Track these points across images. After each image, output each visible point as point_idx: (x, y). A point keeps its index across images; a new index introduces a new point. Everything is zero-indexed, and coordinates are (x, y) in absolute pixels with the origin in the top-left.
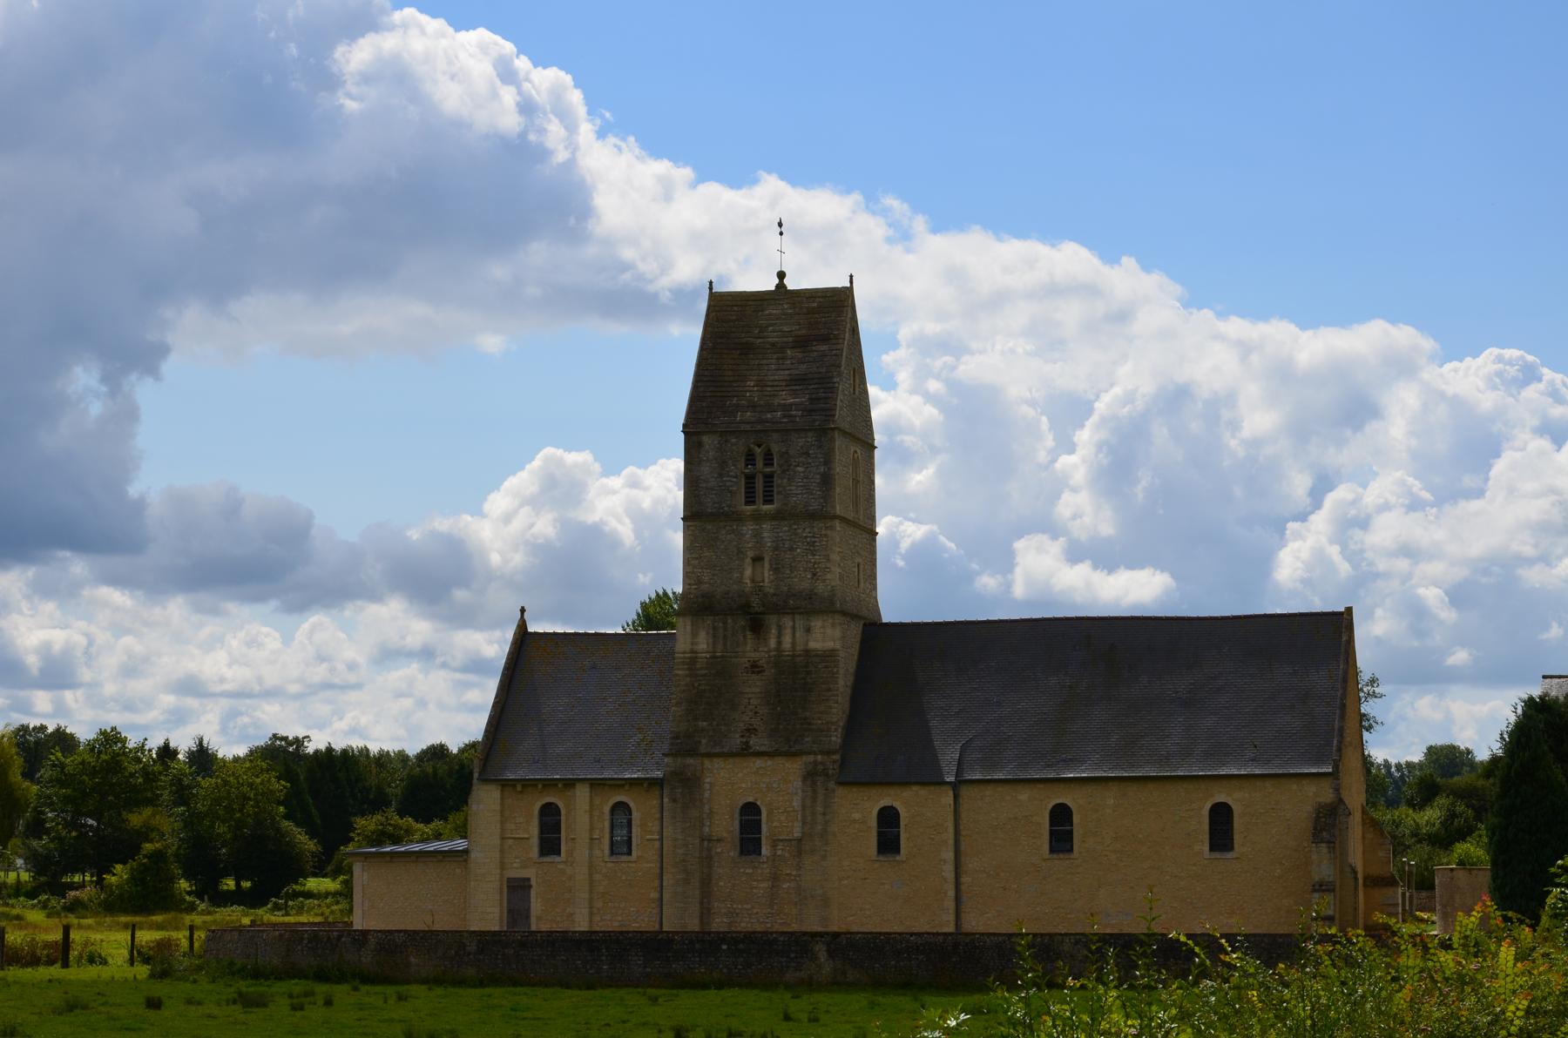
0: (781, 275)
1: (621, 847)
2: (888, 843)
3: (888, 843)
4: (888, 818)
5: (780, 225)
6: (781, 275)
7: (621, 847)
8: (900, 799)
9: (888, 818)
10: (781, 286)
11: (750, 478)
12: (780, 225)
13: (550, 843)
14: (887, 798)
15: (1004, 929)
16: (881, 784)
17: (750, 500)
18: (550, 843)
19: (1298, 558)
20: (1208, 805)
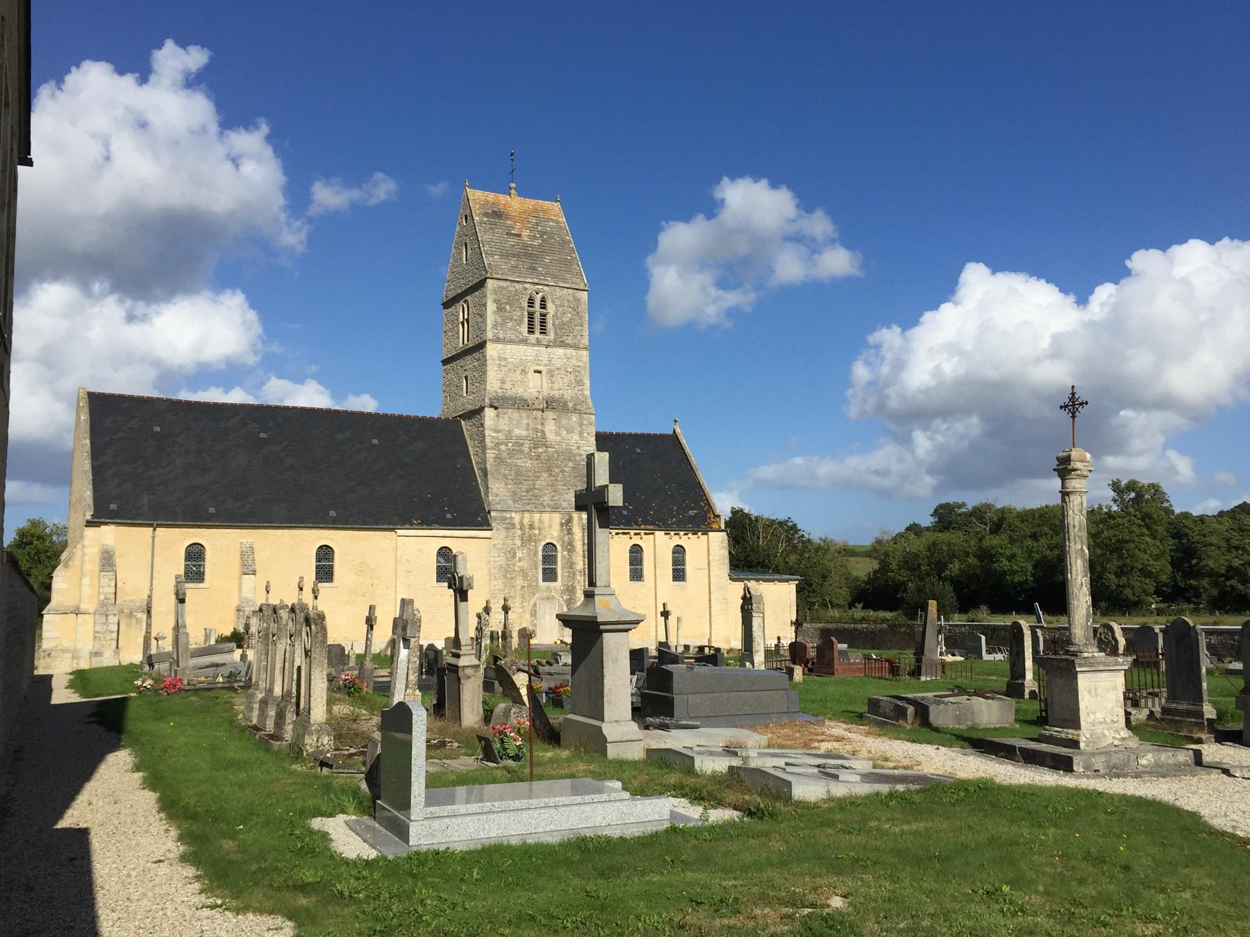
2: (325, 572)
3: (325, 572)
7: (637, 575)
8: (337, 539)
9: (325, 554)
11: (531, 316)
17: (531, 331)
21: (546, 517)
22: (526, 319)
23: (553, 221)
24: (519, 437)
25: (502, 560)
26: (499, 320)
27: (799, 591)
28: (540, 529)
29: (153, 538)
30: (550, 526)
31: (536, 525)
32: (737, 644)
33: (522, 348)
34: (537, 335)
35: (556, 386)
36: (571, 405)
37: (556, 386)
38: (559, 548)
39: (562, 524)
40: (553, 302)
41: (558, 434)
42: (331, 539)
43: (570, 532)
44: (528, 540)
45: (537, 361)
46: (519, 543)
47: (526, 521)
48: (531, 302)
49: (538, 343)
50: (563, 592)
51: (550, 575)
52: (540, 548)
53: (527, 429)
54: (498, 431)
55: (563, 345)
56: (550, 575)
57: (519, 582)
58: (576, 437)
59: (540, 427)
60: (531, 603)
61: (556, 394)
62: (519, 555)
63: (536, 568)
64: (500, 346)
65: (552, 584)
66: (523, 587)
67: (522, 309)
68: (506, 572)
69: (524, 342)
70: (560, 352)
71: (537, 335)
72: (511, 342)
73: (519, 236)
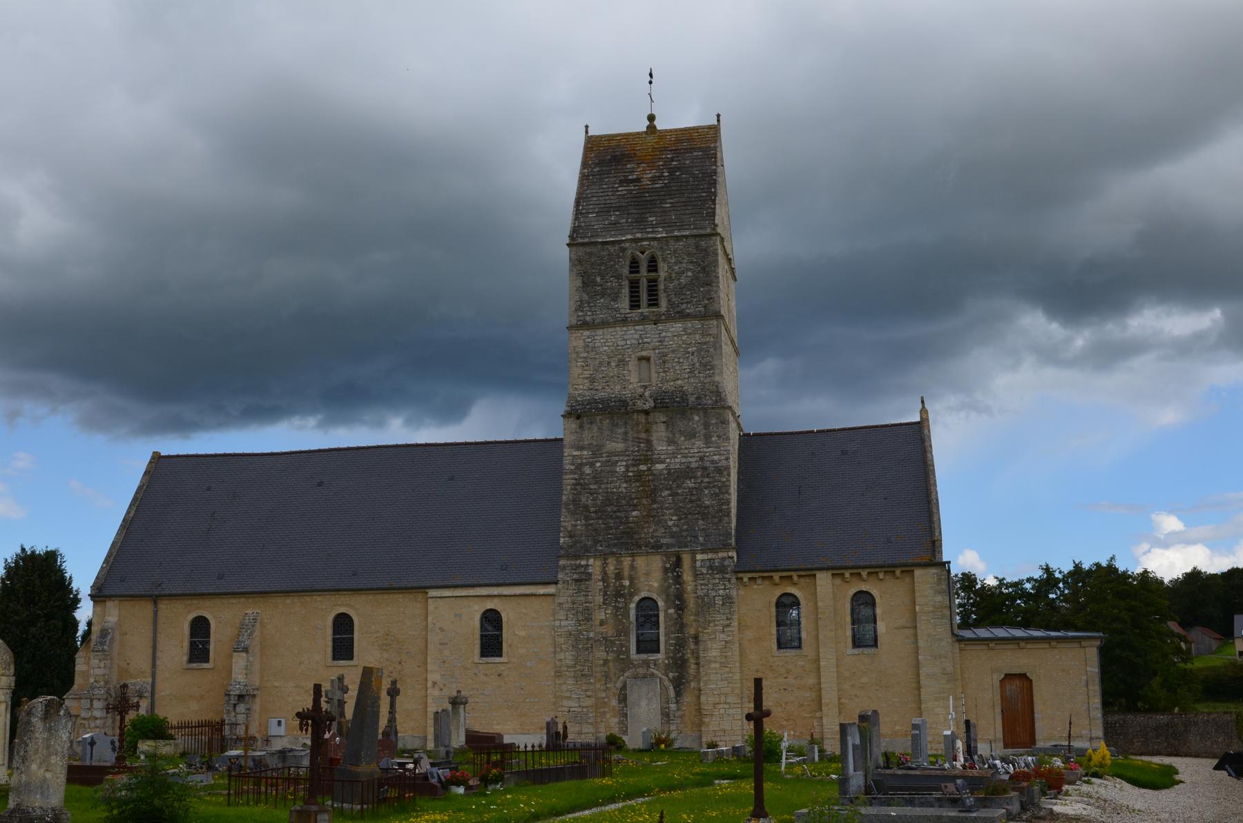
0: (651, 118)
1: (864, 640)
2: (491, 644)
3: (491, 644)
4: (492, 620)
5: (651, 75)
6: (651, 118)
7: (864, 640)
8: (359, 608)
9: (492, 620)
10: (652, 128)
11: (634, 286)
12: (651, 75)
13: (788, 640)
14: (343, 604)
15: (65, 772)
16: (287, 593)
17: (635, 305)
18: (788, 640)
19: (581, 427)
20: (191, 617)
21: (640, 562)
22: (626, 291)
23: (700, 149)
24: (611, 454)
25: (569, 624)
26: (586, 297)
27: (1104, 652)
28: (631, 579)
29: (156, 613)
30: (648, 574)
31: (626, 574)
32: (838, 752)
33: (619, 330)
34: (644, 310)
35: (670, 375)
36: (692, 399)
37: (670, 375)
38: (661, 604)
39: (666, 570)
40: (664, 260)
41: (671, 442)
42: (348, 605)
43: (678, 579)
44: (616, 594)
45: (641, 344)
46: (600, 599)
47: (611, 568)
48: (634, 266)
49: (644, 320)
50: (668, 668)
51: (648, 645)
52: (633, 606)
53: (625, 440)
54: (582, 448)
55: (683, 316)
56: (648, 645)
57: (600, 654)
58: (699, 444)
59: (643, 435)
60: (619, 685)
61: (669, 387)
62: (600, 615)
63: (627, 634)
64: (587, 333)
65: (653, 657)
66: (606, 662)
67: (619, 277)
68: (577, 640)
69: (624, 321)
70: (678, 326)
71: (644, 310)
72: (604, 324)
73: (638, 180)
